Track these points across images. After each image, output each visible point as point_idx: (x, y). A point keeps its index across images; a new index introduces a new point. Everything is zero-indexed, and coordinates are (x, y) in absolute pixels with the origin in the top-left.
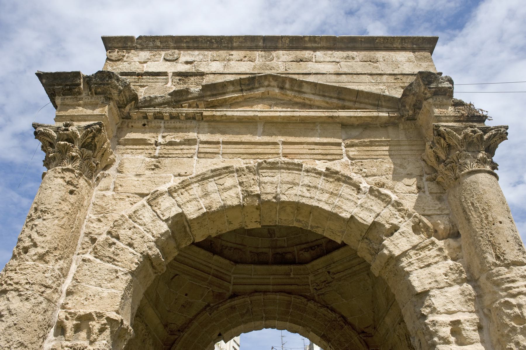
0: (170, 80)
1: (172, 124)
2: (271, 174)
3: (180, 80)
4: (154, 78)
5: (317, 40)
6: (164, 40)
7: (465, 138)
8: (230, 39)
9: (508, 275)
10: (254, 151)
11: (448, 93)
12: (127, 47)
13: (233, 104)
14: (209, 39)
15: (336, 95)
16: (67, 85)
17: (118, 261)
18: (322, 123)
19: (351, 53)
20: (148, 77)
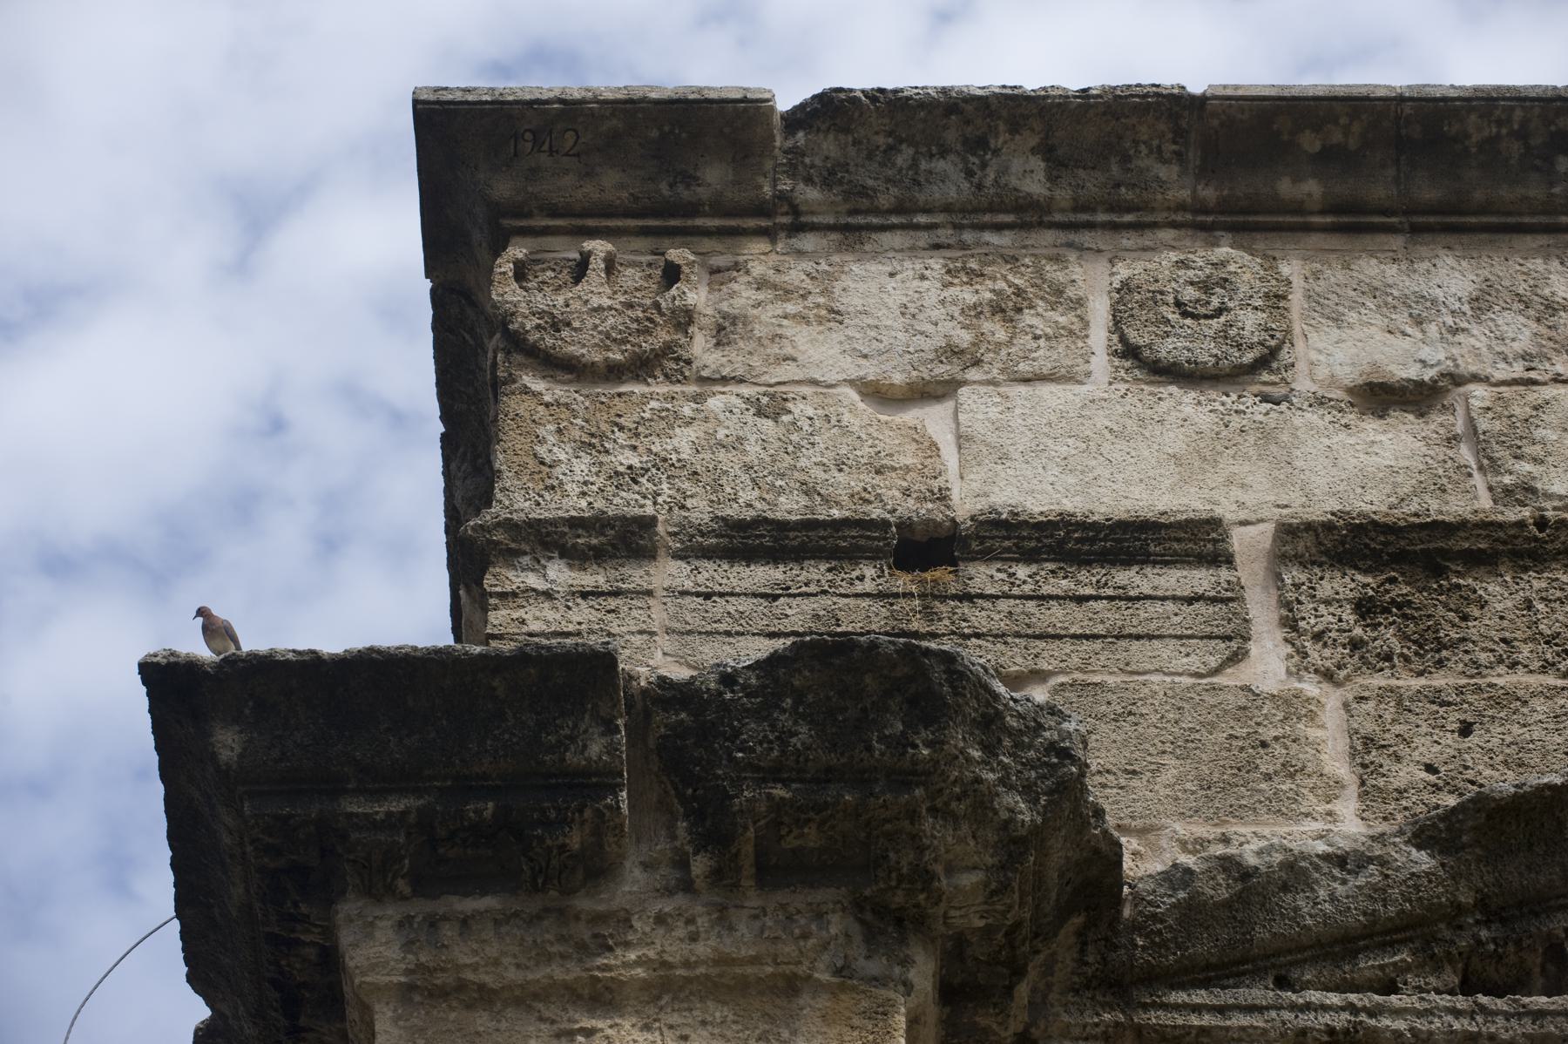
0: (1261, 611)
3: (1365, 608)
4: (1086, 580)
12: (693, 210)
20: (1022, 572)
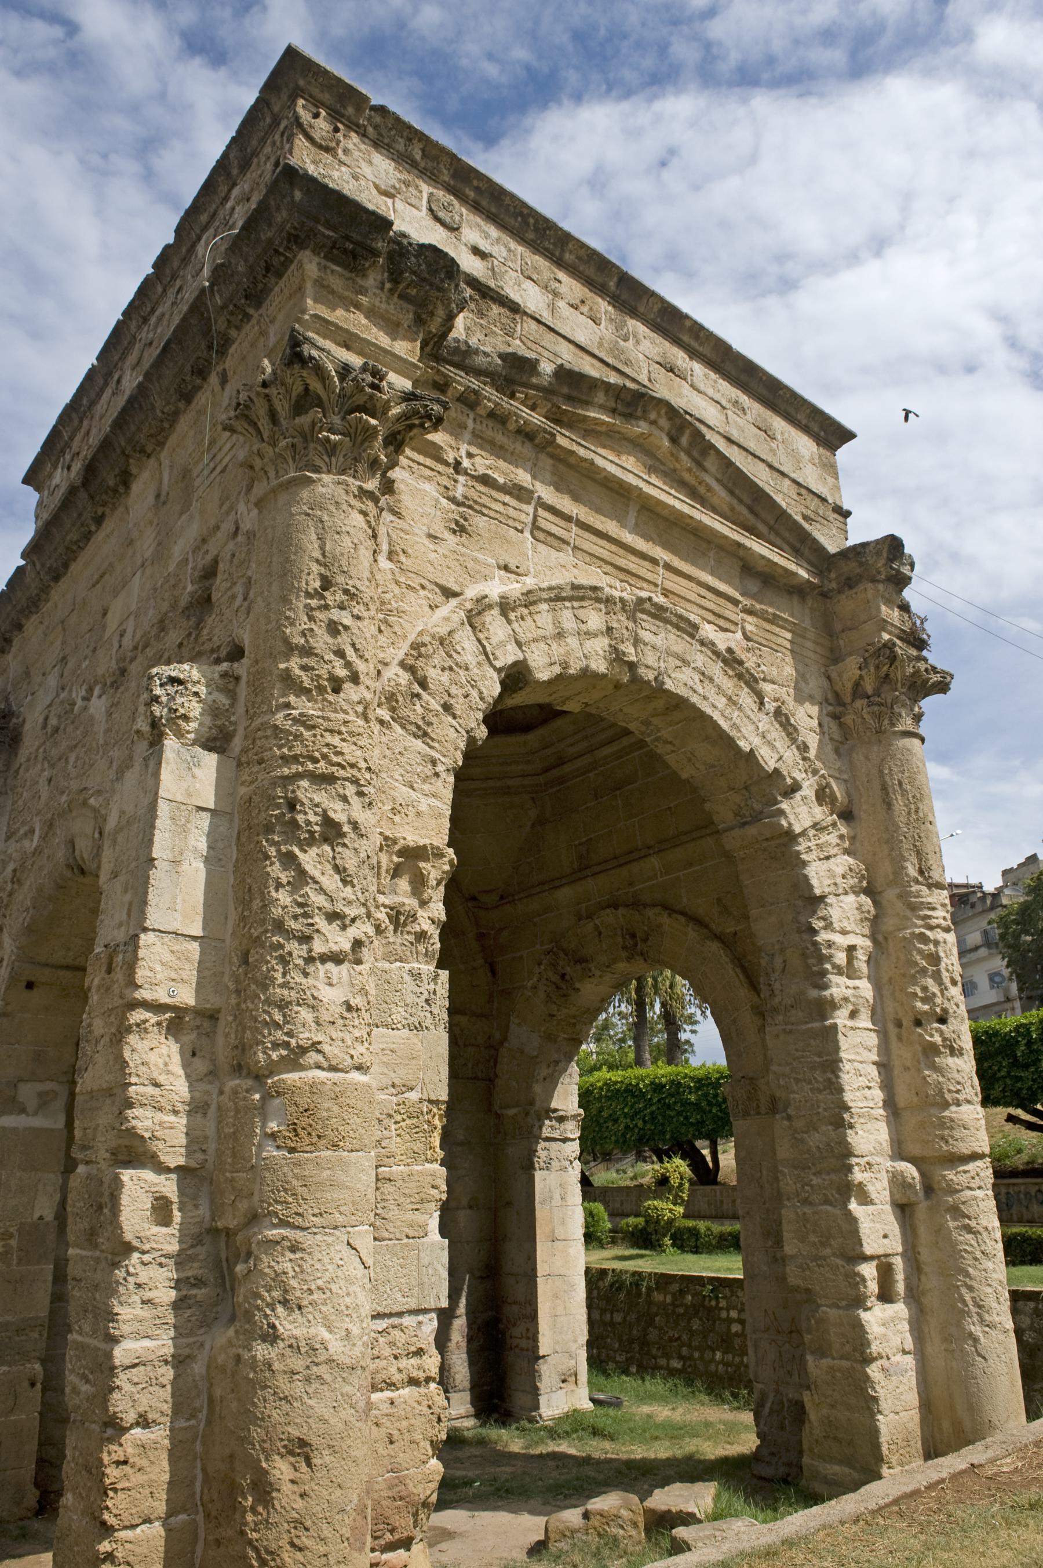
1: (490, 431)
2: (654, 628)
5: (702, 334)
6: (434, 152)
7: (913, 675)
8: (565, 239)
9: (929, 900)
10: (622, 562)
11: (902, 581)
12: (343, 116)
13: (597, 432)
14: (525, 211)
15: (749, 502)
16: (347, 238)
17: (433, 740)
18: (720, 548)
19: (745, 399)
